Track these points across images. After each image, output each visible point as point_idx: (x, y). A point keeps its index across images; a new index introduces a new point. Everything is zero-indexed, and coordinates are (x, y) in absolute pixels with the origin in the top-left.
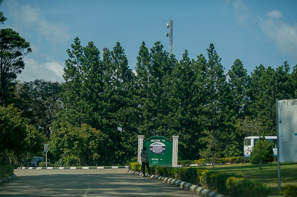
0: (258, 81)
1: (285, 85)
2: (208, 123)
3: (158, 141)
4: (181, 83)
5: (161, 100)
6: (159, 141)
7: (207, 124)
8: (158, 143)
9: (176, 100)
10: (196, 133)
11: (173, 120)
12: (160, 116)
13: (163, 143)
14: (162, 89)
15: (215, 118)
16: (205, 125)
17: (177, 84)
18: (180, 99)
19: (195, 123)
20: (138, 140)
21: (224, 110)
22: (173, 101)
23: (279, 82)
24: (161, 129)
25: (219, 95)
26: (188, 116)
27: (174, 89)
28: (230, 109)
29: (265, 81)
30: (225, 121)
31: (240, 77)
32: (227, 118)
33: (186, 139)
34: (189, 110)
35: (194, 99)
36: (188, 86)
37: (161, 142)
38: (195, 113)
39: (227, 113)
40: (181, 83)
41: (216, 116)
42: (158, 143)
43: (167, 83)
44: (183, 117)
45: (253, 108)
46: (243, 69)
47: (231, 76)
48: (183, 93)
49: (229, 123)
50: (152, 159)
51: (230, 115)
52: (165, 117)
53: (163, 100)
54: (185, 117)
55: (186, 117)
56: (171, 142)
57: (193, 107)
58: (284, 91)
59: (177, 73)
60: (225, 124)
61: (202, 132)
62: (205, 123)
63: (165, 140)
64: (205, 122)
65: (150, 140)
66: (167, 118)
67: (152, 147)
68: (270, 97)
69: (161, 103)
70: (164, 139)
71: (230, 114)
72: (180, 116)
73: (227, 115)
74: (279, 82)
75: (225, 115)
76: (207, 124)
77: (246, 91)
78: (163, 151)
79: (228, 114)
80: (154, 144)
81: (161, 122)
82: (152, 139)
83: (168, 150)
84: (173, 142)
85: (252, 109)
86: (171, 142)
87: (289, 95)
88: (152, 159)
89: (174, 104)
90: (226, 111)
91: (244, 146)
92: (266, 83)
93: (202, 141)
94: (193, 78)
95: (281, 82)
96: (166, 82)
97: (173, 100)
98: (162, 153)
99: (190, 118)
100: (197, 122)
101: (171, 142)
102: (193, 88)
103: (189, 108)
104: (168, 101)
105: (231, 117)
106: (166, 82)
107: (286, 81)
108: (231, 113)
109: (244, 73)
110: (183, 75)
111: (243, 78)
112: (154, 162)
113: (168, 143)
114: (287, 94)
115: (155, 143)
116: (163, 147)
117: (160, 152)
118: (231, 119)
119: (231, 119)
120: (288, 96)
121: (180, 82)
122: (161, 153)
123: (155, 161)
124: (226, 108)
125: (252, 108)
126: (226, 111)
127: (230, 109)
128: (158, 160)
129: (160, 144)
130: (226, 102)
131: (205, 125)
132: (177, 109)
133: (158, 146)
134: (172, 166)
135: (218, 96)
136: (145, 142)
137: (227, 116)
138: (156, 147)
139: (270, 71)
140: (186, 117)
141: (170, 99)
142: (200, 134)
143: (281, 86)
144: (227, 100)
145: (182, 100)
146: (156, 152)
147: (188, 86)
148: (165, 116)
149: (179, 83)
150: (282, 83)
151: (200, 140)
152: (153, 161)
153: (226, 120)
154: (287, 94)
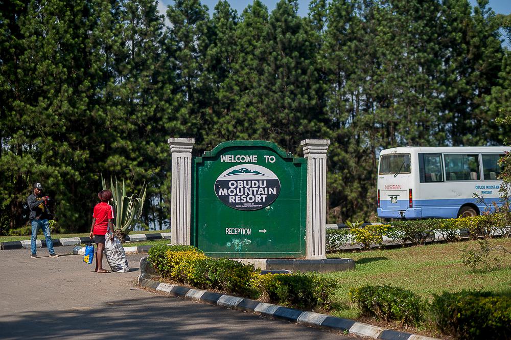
0: (233, 32)
1: (297, 40)
2: (126, 124)
3: (247, 158)
4: (66, 32)
5: (19, 70)
6: (253, 158)
7: (124, 126)
8: (249, 167)
9: (55, 71)
10: (101, 145)
11: (48, 116)
12: (19, 106)
13: (268, 166)
14: (20, 44)
15: (144, 113)
16: (121, 127)
17: (58, 33)
18: (64, 67)
19: (98, 125)
20: (170, 155)
21: (163, 94)
22: (48, 73)
23: (284, 33)
24: (21, 136)
25: (151, 61)
26: (83, 108)
27: (51, 44)
28: (174, 92)
29: (251, 31)
30: (164, 120)
31: (194, 22)
32: (168, 113)
33: (80, 160)
34: (85, 95)
35: (96, 70)
36: (81, 39)
37: (261, 162)
38: (93, 102)
39: (169, 101)
40: (66, 32)
41: (146, 108)
42: (249, 167)
43: (33, 31)
44: (71, 109)
45: (226, 91)
46: (200, 5)
47: (174, 21)
48: (71, 55)
49: (173, 125)
50: (228, 231)
51: (175, 106)
52: (31, 110)
53: (26, 71)
54: (76, 110)
55: (78, 108)
56: (298, 165)
57: (93, 87)
58: (296, 53)
59: (55, 7)
60: (165, 125)
61: (115, 145)
62: (120, 125)
63: (279, 156)
64: (119, 121)
65: (216, 157)
66: (34, 112)
67: (225, 184)
68: (266, 67)
69: (19, 76)
70: (272, 151)
71: (176, 104)
72: (66, 106)
73: (167, 105)
74: (284, 33)
75: (163, 105)
76: (124, 126)
77: (211, 52)
78: (270, 198)
79: (171, 104)
80: (235, 172)
81: (20, 122)
82: (225, 151)
83: (288, 197)
84: (310, 162)
85: (224, 93)
86: (298, 165)
87: (306, 61)
88: (228, 231)
89: (51, 79)
90: (165, 97)
91: (379, 176)
92: (253, 36)
93: (114, 165)
94: (92, 20)
95: (290, 33)
96: (29, 28)
97: (48, 70)
98: (264, 204)
99: (88, 111)
100: (104, 122)
101: (301, 165)
102: (92, 44)
103: (84, 90)
104: (37, 73)
105: (177, 110)
106: (29, 28)
107: (298, 32)
108: (178, 101)
109: (202, 13)
110: (69, 13)
111: (201, 25)
112: (236, 242)
113: (289, 169)
114: (303, 59)
115: (238, 168)
116: (270, 183)
117: (258, 203)
118: (178, 115)
119: (178, 115)
120: (303, 64)
121: (63, 29)
122: (263, 208)
123: (240, 237)
124: (165, 89)
125: (225, 90)
126: (165, 97)
127: (174, 92)
128: (249, 232)
129: (256, 172)
130: (166, 77)
131: (121, 127)
132: (58, 91)
133: (248, 177)
134: (305, 253)
135: (148, 62)
136: (199, 164)
137: (168, 108)
138: (240, 184)
139: (260, 9)
140: (78, 108)
141: (41, 68)
142: (110, 148)
143: (290, 41)
144: (168, 73)
145: (68, 71)
146: (242, 204)
147: (81, 39)
148: (31, 107)
149: (61, 31)
150: (293, 37)
151: (111, 163)
152: (230, 238)
153: (166, 117)
154: (303, 59)
